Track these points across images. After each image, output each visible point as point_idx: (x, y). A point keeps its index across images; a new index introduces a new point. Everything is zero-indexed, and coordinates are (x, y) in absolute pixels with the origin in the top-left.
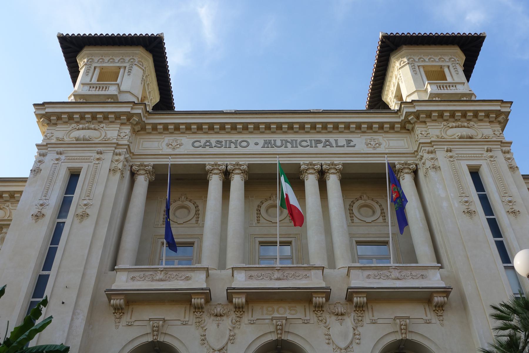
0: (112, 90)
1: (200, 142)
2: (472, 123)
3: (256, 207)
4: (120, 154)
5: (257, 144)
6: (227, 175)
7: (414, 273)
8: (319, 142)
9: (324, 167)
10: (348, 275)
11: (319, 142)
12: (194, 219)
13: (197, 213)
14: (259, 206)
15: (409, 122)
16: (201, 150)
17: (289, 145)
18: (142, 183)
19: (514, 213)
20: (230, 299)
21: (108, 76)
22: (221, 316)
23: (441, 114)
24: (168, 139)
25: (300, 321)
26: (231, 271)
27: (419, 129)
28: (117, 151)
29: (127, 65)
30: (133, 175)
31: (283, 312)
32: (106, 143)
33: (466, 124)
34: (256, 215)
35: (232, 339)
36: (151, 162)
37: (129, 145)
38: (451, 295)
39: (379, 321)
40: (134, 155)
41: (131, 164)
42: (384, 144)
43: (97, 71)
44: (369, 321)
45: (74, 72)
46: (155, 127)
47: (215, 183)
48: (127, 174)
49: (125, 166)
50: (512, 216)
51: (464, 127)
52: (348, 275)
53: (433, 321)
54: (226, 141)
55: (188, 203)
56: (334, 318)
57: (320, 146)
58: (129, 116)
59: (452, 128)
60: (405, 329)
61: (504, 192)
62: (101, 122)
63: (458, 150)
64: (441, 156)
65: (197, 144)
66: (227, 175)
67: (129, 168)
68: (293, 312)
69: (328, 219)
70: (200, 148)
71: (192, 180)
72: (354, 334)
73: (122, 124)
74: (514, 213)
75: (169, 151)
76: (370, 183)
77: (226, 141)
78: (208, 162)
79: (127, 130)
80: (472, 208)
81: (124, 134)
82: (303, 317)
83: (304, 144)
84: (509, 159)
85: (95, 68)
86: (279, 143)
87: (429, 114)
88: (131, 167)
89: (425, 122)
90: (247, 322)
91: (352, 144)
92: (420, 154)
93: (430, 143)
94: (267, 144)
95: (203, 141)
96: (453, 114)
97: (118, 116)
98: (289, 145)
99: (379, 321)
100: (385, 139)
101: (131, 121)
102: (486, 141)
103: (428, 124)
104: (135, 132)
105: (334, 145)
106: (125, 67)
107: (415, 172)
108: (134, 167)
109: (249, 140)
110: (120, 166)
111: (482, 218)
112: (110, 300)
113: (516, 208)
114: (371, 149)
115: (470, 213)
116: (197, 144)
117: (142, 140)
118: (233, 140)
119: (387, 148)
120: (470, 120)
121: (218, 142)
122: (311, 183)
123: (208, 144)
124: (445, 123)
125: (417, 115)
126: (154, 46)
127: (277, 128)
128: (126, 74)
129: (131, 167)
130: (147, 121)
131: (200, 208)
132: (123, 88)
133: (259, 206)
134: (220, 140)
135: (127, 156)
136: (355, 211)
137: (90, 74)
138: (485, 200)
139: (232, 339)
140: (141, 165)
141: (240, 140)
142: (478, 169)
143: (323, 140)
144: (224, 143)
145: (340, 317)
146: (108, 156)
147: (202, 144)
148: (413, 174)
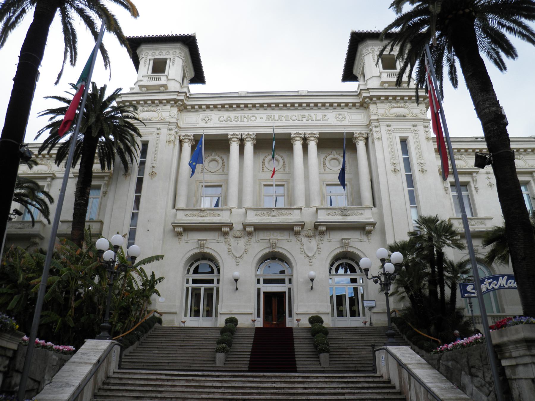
0: (163, 81)
1: (223, 117)
2: (407, 104)
3: (261, 160)
4: (172, 130)
5: (261, 118)
6: (242, 142)
7: (356, 211)
8: (304, 116)
9: (243, 136)
10: (317, 212)
11: (304, 116)
12: (222, 169)
13: (223, 165)
14: (264, 160)
15: (365, 103)
16: (224, 124)
17: (283, 119)
18: (187, 147)
19: (423, 171)
20: (245, 227)
21: (159, 67)
22: (239, 237)
23: (387, 98)
24: (202, 115)
25: (286, 241)
26: (244, 210)
27: (372, 107)
28: (170, 127)
29: (171, 57)
30: (181, 141)
31: (274, 236)
32: (162, 122)
33: (403, 105)
34: (261, 166)
35: (246, 251)
36: (192, 133)
37: (177, 123)
38: (376, 226)
39: (332, 241)
40: (180, 128)
41: (179, 134)
42: (348, 118)
43: (152, 62)
44: (327, 241)
45: (137, 64)
46: (193, 107)
47: (235, 147)
48: (177, 142)
49: (175, 137)
50: (421, 174)
51: (402, 107)
52: (317, 212)
53: (364, 240)
54: (241, 116)
55: (217, 158)
56: (306, 239)
57: (305, 119)
58: (176, 101)
59: (393, 108)
60: (346, 245)
61: (420, 156)
62: (158, 106)
63: (395, 125)
64: (383, 128)
65: (221, 119)
66: (242, 142)
67: (178, 138)
68: (282, 235)
69: (310, 169)
70: (224, 122)
71: (218, 144)
72: (318, 248)
73: (172, 106)
74: (423, 171)
75: (203, 124)
76: (338, 144)
77: (241, 116)
78: (230, 132)
79: (175, 110)
80: (398, 168)
81: (173, 114)
82: (288, 239)
83: (294, 118)
84: (427, 132)
85: (150, 60)
86: (276, 118)
87: (379, 98)
88: (180, 137)
89: (376, 103)
90: (255, 241)
91: (326, 118)
92: (371, 127)
93: (378, 120)
94: (269, 118)
95: (226, 116)
96: (395, 98)
97: (168, 101)
98: (283, 119)
99: (332, 241)
100: (349, 114)
101: (177, 104)
102: (415, 118)
103: (378, 105)
104: (180, 111)
105: (314, 119)
106: (170, 59)
107: (367, 139)
108: (181, 137)
109: (256, 115)
110: (172, 138)
111: (403, 173)
112: (174, 229)
113: (425, 168)
114: (338, 122)
115: (395, 171)
116: (221, 119)
117: (185, 116)
118: (246, 115)
119: (350, 121)
120: (406, 102)
121: (236, 117)
122: (298, 146)
123: (229, 119)
124: (389, 104)
125: (371, 98)
126: (189, 43)
127: (276, 106)
128: (171, 64)
129: (180, 137)
130: (188, 103)
131: (225, 161)
132: (169, 77)
133: (264, 160)
134: (237, 115)
135: (177, 130)
136: (327, 163)
137: (147, 66)
138: (407, 162)
139: (246, 251)
140: (186, 136)
141: (251, 115)
142: (406, 140)
143: (307, 114)
144: (239, 118)
145: (310, 238)
146: (164, 131)
147: (225, 119)
148: (365, 140)
